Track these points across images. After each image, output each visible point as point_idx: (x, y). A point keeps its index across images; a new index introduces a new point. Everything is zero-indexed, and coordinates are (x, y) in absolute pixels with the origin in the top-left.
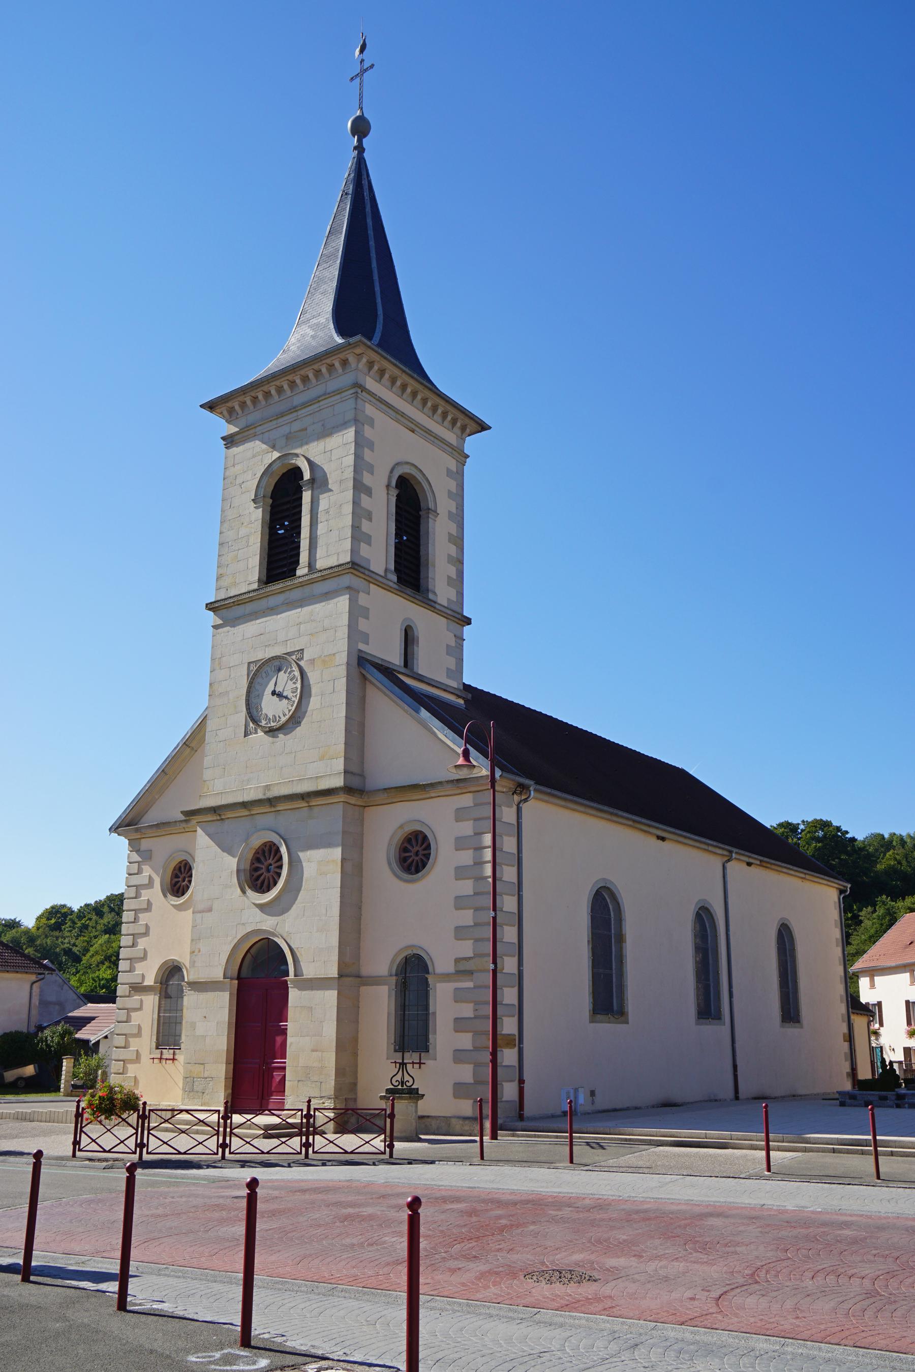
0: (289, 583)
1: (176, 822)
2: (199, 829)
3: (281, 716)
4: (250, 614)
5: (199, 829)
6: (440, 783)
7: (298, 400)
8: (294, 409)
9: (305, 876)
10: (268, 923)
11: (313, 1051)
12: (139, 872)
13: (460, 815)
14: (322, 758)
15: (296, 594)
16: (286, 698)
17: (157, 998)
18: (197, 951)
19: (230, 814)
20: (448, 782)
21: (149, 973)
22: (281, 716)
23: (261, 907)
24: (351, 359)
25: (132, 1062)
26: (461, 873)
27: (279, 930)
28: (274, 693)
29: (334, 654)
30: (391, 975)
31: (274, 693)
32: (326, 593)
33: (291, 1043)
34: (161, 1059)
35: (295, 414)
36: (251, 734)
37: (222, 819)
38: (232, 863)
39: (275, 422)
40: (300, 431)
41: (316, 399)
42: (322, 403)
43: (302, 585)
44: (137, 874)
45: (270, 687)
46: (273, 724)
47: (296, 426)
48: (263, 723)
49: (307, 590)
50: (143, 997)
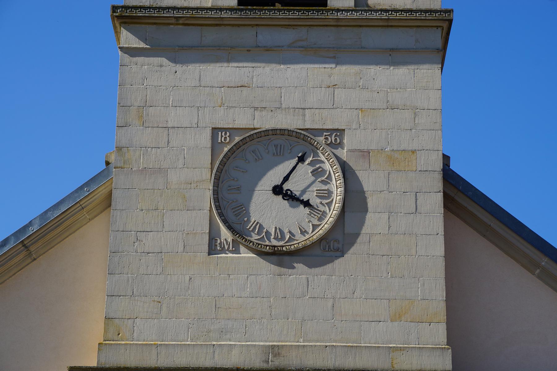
22: (297, 232)
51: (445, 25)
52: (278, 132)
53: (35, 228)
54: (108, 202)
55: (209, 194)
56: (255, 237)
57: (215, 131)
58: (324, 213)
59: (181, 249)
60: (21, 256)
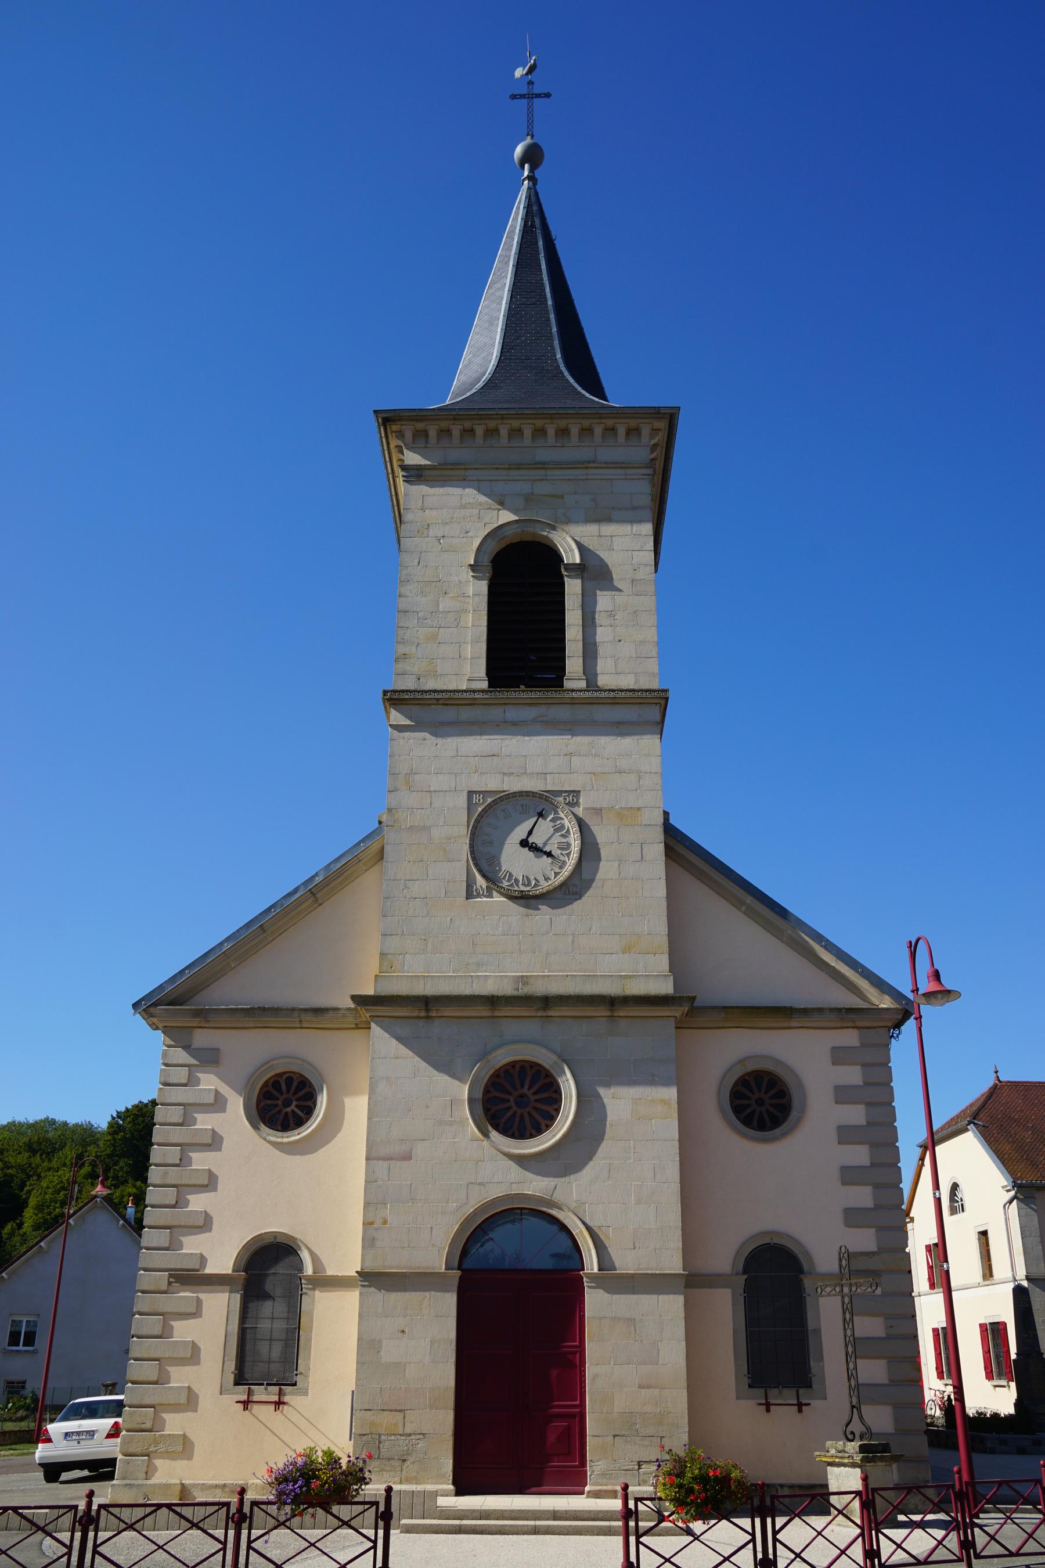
0: (552, 694)
1: (293, 1009)
2: (373, 1025)
3: (541, 879)
4: (474, 723)
5: (373, 1025)
6: (820, 1010)
7: (605, 454)
8: (542, 465)
9: (609, 1119)
10: (535, 1186)
11: (641, 1387)
12: (191, 1082)
13: (839, 1057)
14: (627, 950)
15: (562, 713)
16: (549, 854)
17: (237, 1298)
18: (378, 1223)
19: (448, 1012)
20: (831, 1010)
21: (222, 1255)
22: (541, 879)
23: (521, 1160)
24: (646, 431)
25: (176, 1408)
26: (846, 1135)
27: (558, 1197)
28: (524, 843)
29: (639, 809)
30: (737, 1274)
31: (524, 843)
32: (619, 723)
33: (595, 1377)
34: (662, 1437)
35: (543, 472)
36: (478, 896)
37: (431, 1017)
38: (465, 1091)
39: (504, 472)
40: (551, 496)
41: (583, 463)
42: (590, 471)
43: (573, 702)
44: (185, 1085)
45: (520, 832)
46: (522, 888)
47: (541, 488)
48: (505, 884)
49: (582, 712)
50: (202, 1296)
51: (663, 702)
54: (381, 855)
55: (466, 848)
57: (470, 793)
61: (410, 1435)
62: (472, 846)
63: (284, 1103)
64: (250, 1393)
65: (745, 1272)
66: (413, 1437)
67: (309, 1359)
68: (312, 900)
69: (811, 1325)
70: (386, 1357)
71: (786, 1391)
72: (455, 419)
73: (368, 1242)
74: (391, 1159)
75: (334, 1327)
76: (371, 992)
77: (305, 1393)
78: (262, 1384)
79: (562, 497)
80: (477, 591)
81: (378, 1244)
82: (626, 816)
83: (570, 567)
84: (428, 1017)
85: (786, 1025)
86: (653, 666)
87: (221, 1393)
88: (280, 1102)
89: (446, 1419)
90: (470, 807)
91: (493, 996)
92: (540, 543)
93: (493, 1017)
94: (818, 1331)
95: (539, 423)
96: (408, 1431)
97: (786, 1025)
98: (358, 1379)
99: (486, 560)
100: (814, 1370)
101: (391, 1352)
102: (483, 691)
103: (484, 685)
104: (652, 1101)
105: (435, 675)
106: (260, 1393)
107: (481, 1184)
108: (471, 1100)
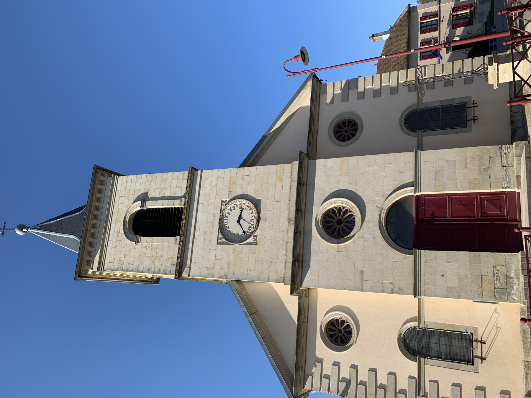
14: (281, 180)
18: (391, 286)
21: (408, 367)
22: (252, 215)
24: (102, 178)
44: (329, 380)
51: (193, 170)
52: (434, 344)
53: (245, 310)
54: (239, 282)
55: (238, 245)
56: (252, 230)
57: (218, 243)
58: (241, 205)
59: (255, 255)
60: (255, 316)
61: (494, 273)
62: (237, 243)
63: (340, 334)
64: (477, 357)
65: (415, 131)
66: (495, 272)
67: (459, 326)
68: (254, 315)
69: (439, 104)
70: (455, 284)
71: (468, 112)
72: (84, 249)
73: (401, 291)
74: (362, 280)
75: (445, 312)
76: (289, 287)
77: (475, 329)
78: (473, 350)
79: (119, 209)
80: (144, 240)
81: (401, 287)
82: (233, 182)
83: (142, 206)
84: (302, 262)
85: (316, 122)
86: (181, 173)
87: (478, 373)
88: (340, 335)
89: (486, 257)
90: (223, 243)
91: (294, 232)
92: (134, 218)
93: (304, 233)
94: (441, 101)
95: (91, 217)
96: (492, 274)
97: (316, 122)
98: (466, 298)
99: (135, 237)
100: (459, 102)
101: (453, 282)
102: (180, 238)
103: (178, 237)
104: (341, 167)
105: (173, 258)
106: (477, 352)
107: (374, 238)
108: (338, 243)
